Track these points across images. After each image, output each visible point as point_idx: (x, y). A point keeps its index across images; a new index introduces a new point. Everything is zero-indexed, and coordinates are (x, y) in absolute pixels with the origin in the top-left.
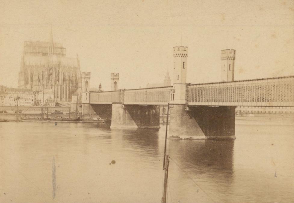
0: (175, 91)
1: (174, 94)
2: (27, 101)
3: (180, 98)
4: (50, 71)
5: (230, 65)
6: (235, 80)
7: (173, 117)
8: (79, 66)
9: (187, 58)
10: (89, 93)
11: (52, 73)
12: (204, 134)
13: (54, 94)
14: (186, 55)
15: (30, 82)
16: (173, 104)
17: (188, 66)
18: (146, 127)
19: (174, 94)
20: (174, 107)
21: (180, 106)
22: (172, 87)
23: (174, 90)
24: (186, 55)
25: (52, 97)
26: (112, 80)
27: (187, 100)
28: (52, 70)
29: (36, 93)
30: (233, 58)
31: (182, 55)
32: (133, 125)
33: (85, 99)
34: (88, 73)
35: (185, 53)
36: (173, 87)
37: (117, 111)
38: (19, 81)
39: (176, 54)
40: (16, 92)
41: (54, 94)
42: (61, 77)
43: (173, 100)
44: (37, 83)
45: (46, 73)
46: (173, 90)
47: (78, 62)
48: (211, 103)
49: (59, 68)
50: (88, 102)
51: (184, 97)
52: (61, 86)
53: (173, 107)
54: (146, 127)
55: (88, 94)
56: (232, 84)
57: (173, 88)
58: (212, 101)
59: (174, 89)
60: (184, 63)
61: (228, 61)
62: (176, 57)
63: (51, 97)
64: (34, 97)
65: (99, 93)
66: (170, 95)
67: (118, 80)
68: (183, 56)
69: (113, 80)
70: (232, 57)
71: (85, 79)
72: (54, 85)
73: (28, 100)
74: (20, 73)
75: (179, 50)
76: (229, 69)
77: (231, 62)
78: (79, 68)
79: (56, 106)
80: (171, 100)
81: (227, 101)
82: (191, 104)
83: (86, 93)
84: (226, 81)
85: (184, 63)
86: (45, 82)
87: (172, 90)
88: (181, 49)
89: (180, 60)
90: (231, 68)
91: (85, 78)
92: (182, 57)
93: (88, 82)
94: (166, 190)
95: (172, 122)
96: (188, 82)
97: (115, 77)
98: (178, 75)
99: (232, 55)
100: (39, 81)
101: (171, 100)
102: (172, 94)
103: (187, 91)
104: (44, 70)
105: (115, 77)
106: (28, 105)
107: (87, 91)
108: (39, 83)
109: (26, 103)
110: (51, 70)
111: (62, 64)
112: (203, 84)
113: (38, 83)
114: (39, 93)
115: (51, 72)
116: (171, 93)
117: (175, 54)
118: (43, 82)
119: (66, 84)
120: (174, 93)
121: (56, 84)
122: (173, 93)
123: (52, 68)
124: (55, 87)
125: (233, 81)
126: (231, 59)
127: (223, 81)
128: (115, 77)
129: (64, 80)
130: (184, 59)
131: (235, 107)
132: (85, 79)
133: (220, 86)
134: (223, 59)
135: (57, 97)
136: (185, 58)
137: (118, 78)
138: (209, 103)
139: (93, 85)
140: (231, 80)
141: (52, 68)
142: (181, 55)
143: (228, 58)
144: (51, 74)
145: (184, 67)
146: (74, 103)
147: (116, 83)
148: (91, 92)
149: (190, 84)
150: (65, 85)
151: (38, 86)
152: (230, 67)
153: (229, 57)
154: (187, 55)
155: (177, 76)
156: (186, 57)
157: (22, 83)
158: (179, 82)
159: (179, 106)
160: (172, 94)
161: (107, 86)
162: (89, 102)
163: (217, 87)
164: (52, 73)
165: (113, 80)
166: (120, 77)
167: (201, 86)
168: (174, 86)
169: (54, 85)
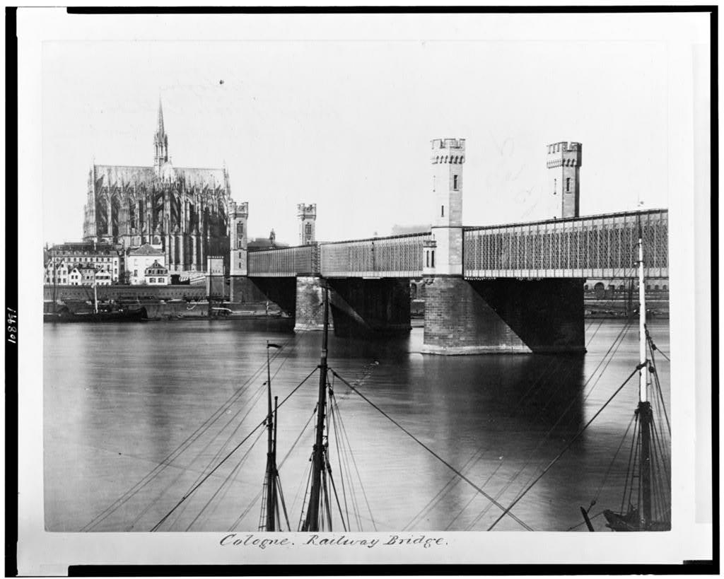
1: (433, 252)
2: (99, 274)
4: (157, 200)
5: (568, 179)
6: (582, 214)
7: (433, 307)
9: (464, 164)
10: (245, 252)
12: (521, 342)
14: (462, 158)
16: (433, 276)
19: (433, 252)
20: (434, 281)
22: (430, 234)
23: (435, 242)
24: (462, 158)
26: (301, 220)
28: (164, 198)
29: (123, 255)
30: (575, 163)
31: (452, 158)
33: (238, 269)
34: (243, 204)
35: (456, 153)
36: (432, 235)
38: (87, 224)
39: (438, 158)
42: (185, 215)
44: (129, 230)
45: (149, 205)
46: (432, 242)
47: (226, 176)
48: (553, 270)
49: (180, 192)
51: (457, 258)
52: (185, 235)
53: (432, 282)
55: (244, 253)
56: (577, 224)
57: (431, 238)
58: (500, 267)
59: (433, 240)
60: (456, 176)
61: (563, 169)
62: (437, 163)
63: (159, 262)
64: (118, 263)
66: (425, 254)
67: (315, 219)
68: (454, 160)
69: (303, 219)
70: (573, 161)
71: (235, 218)
72: (167, 233)
73: (102, 271)
75: (444, 147)
76: (565, 190)
78: (229, 192)
79: (173, 283)
80: (428, 266)
83: (240, 251)
84: (559, 217)
85: (456, 176)
86: (146, 227)
89: (446, 170)
91: (236, 215)
92: (450, 162)
93: (244, 226)
94: (70, 529)
95: (430, 318)
97: (308, 213)
98: (443, 207)
99: (573, 156)
101: (428, 266)
102: (428, 252)
104: (144, 199)
105: (308, 213)
107: (242, 245)
108: (133, 229)
109: (97, 278)
110: (161, 199)
111: (187, 183)
112: (508, 226)
113: (131, 229)
114: (131, 253)
115: (160, 202)
117: (434, 159)
118: (143, 226)
119: (198, 230)
120: (433, 249)
121: (172, 231)
122: (430, 250)
123: (162, 195)
124: (170, 238)
125: (577, 218)
126: (572, 166)
128: (307, 213)
129: (193, 220)
132: (235, 218)
133: (574, 228)
134: (551, 165)
135: (177, 262)
136: (458, 165)
137: (314, 213)
138: (523, 271)
139: (255, 231)
140: (571, 215)
141: (162, 195)
142: (449, 160)
143: (565, 163)
144: (162, 207)
145: (455, 187)
150: (194, 232)
151: (131, 236)
152: (568, 184)
153: (567, 160)
154: (463, 160)
156: (460, 163)
157: (93, 230)
159: (446, 281)
160: (428, 252)
161: (290, 237)
162: (248, 273)
163: (566, 231)
164: (163, 205)
165: (303, 219)
167: (503, 231)
168: (434, 231)
169: (167, 233)
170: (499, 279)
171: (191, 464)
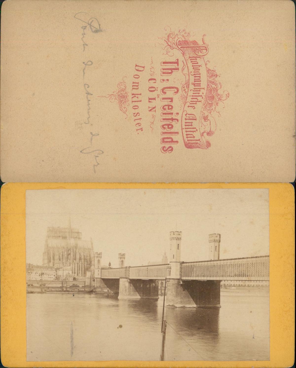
0: (171, 268)
1: (170, 271)
2: (50, 276)
3: (175, 274)
5: (216, 247)
6: (220, 259)
8: (92, 247)
9: (181, 241)
10: (100, 270)
11: (70, 253)
13: (72, 270)
14: (180, 238)
15: (52, 261)
16: (170, 279)
17: (181, 247)
18: (147, 297)
19: (170, 271)
20: (170, 281)
21: (175, 280)
22: (169, 264)
23: (171, 267)
24: (180, 238)
25: (71, 273)
26: (119, 259)
27: (181, 275)
28: (70, 251)
29: (57, 270)
30: (218, 241)
31: (177, 238)
32: (136, 296)
33: (97, 275)
34: (100, 253)
35: (179, 236)
36: (170, 265)
37: (124, 284)
38: (44, 260)
39: (172, 238)
40: (41, 269)
41: (72, 270)
42: (78, 257)
43: (170, 275)
44: (58, 262)
45: (66, 253)
46: (170, 267)
47: (92, 244)
48: (201, 277)
49: (76, 249)
50: (100, 277)
51: (178, 273)
52: (78, 264)
53: (169, 281)
54: (147, 297)
55: (100, 270)
56: (218, 262)
57: (169, 266)
58: (201, 276)
59: (170, 266)
60: (178, 245)
61: (214, 243)
62: (172, 240)
64: (55, 272)
65: (109, 270)
66: (167, 271)
67: (125, 259)
68: (178, 239)
69: (121, 259)
70: (218, 240)
71: (97, 258)
73: (51, 275)
74: (44, 253)
75: (174, 234)
76: (215, 250)
77: (217, 244)
78: (93, 249)
79: (73, 280)
81: (214, 276)
82: (184, 278)
83: (98, 269)
84: (213, 259)
85: (178, 245)
86: (64, 261)
87: (168, 267)
88: (176, 233)
89: (175, 242)
90: (217, 249)
92: (177, 240)
93: (100, 261)
95: (169, 293)
96: (182, 260)
97: (122, 256)
98: (174, 255)
99: (218, 238)
100: (60, 260)
101: (168, 275)
102: (168, 270)
103: (181, 268)
104: (64, 251)
105: (122, 256)
106: (51, 280)
107: (99, 268)
108: (60, 261)
109: (49, 278)
110: (70, 251)
111: (78, 246)
112: (194, 262)
113: (59, 262)
114: (60, 269)
115: (69, 252)
116: (167, 270)
118: (63, 260)
119: (82, 262)
120: (170, 270)
121: (73, 262)
122: (169, 270)
123: (70, 249)
124: (73, 265)
125: (219, 260)
126: (217, 242)
127: (210, 260)
128: (122, 257)
129: (80, 259)
130: (178, 242)
131: (220, 281)
132: (97, 258)
133: (208, 264)
135: (75, 273)
136: (180, 241)
137: (124, 257)
138: (199, 278)
139: (104, 263)
140: (217, 259)
141: (70, 249)
142: (176, 239)
143: (215, 241)
144: (70, 254)
145: (178, 248)
146: (89, 278)
147: (122, 261)
148: (102, 269)
149: (183, 263)
150: (81, 263)
151: (59, 264)
152: (216, 248)
153: (216, 240)
154: (181, 239)
155: (173, 255)
156: (180, 240)
157: (46, 261)
158: (174, 260)
159: (174, 281)
160: (168, 270)
161: (116, 264)
162: (101, 277)
163: (205, 265)
164: (70, 253)
165: (121, 259)
166: (126, 256)
167: (192, 264)
168: (170, 263)
169: (71, 263)
170: (208, 281)
171: (26, 328)
